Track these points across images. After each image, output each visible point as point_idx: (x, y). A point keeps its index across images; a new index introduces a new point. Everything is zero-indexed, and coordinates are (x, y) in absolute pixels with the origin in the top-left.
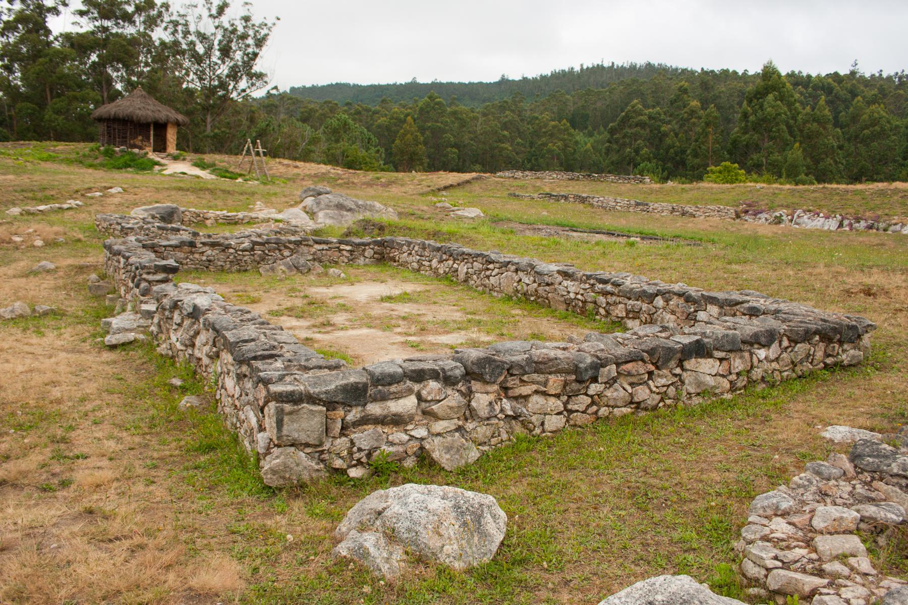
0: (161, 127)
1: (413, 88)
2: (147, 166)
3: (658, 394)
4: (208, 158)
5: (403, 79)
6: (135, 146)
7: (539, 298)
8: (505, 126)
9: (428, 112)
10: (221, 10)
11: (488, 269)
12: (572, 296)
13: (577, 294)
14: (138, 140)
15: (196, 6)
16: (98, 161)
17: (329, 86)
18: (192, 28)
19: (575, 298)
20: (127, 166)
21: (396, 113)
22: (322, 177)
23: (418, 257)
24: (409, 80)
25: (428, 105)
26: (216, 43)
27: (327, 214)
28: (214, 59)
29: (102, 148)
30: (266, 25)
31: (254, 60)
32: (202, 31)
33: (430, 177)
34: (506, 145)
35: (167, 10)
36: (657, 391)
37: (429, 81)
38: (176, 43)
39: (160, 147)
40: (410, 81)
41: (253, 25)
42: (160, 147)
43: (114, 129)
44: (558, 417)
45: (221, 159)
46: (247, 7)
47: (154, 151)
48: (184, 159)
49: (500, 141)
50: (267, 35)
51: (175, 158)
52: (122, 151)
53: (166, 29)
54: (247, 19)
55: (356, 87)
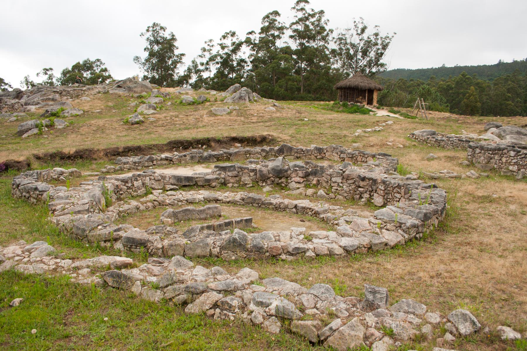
0: (371, 91)
1: (443, 71)
2: (365, 112)
5: (436, 64)
6: (358, 102)
8: (509, 91)
9: (461, 84)
10: (363, 30)
14: (360, 99)
16: (340, 110)
17: (393, 70)
18: (348, 41)
20: (355, 112)
21: (442, 84)
22: (448, 119)
24: (440, 66)
26: (360, 48)
27: (512, 137)
30: (388, 37)
31: (381, 56)
32: (353, 42)
33: (513, 119)
34: (510, 102)
35: (332, 33)
37: (453, 66)
39: (370, 102)
41: (381, 38)
42: (370, 102)
43: (348, 93)
45: (404, 110)
46: (377, 28)
48: (383, 109)
49: (506, 100)
50: (389, 43)
52: (351, 104)
53: (335, 42)
54: (376, 35)
55: (409, 70)
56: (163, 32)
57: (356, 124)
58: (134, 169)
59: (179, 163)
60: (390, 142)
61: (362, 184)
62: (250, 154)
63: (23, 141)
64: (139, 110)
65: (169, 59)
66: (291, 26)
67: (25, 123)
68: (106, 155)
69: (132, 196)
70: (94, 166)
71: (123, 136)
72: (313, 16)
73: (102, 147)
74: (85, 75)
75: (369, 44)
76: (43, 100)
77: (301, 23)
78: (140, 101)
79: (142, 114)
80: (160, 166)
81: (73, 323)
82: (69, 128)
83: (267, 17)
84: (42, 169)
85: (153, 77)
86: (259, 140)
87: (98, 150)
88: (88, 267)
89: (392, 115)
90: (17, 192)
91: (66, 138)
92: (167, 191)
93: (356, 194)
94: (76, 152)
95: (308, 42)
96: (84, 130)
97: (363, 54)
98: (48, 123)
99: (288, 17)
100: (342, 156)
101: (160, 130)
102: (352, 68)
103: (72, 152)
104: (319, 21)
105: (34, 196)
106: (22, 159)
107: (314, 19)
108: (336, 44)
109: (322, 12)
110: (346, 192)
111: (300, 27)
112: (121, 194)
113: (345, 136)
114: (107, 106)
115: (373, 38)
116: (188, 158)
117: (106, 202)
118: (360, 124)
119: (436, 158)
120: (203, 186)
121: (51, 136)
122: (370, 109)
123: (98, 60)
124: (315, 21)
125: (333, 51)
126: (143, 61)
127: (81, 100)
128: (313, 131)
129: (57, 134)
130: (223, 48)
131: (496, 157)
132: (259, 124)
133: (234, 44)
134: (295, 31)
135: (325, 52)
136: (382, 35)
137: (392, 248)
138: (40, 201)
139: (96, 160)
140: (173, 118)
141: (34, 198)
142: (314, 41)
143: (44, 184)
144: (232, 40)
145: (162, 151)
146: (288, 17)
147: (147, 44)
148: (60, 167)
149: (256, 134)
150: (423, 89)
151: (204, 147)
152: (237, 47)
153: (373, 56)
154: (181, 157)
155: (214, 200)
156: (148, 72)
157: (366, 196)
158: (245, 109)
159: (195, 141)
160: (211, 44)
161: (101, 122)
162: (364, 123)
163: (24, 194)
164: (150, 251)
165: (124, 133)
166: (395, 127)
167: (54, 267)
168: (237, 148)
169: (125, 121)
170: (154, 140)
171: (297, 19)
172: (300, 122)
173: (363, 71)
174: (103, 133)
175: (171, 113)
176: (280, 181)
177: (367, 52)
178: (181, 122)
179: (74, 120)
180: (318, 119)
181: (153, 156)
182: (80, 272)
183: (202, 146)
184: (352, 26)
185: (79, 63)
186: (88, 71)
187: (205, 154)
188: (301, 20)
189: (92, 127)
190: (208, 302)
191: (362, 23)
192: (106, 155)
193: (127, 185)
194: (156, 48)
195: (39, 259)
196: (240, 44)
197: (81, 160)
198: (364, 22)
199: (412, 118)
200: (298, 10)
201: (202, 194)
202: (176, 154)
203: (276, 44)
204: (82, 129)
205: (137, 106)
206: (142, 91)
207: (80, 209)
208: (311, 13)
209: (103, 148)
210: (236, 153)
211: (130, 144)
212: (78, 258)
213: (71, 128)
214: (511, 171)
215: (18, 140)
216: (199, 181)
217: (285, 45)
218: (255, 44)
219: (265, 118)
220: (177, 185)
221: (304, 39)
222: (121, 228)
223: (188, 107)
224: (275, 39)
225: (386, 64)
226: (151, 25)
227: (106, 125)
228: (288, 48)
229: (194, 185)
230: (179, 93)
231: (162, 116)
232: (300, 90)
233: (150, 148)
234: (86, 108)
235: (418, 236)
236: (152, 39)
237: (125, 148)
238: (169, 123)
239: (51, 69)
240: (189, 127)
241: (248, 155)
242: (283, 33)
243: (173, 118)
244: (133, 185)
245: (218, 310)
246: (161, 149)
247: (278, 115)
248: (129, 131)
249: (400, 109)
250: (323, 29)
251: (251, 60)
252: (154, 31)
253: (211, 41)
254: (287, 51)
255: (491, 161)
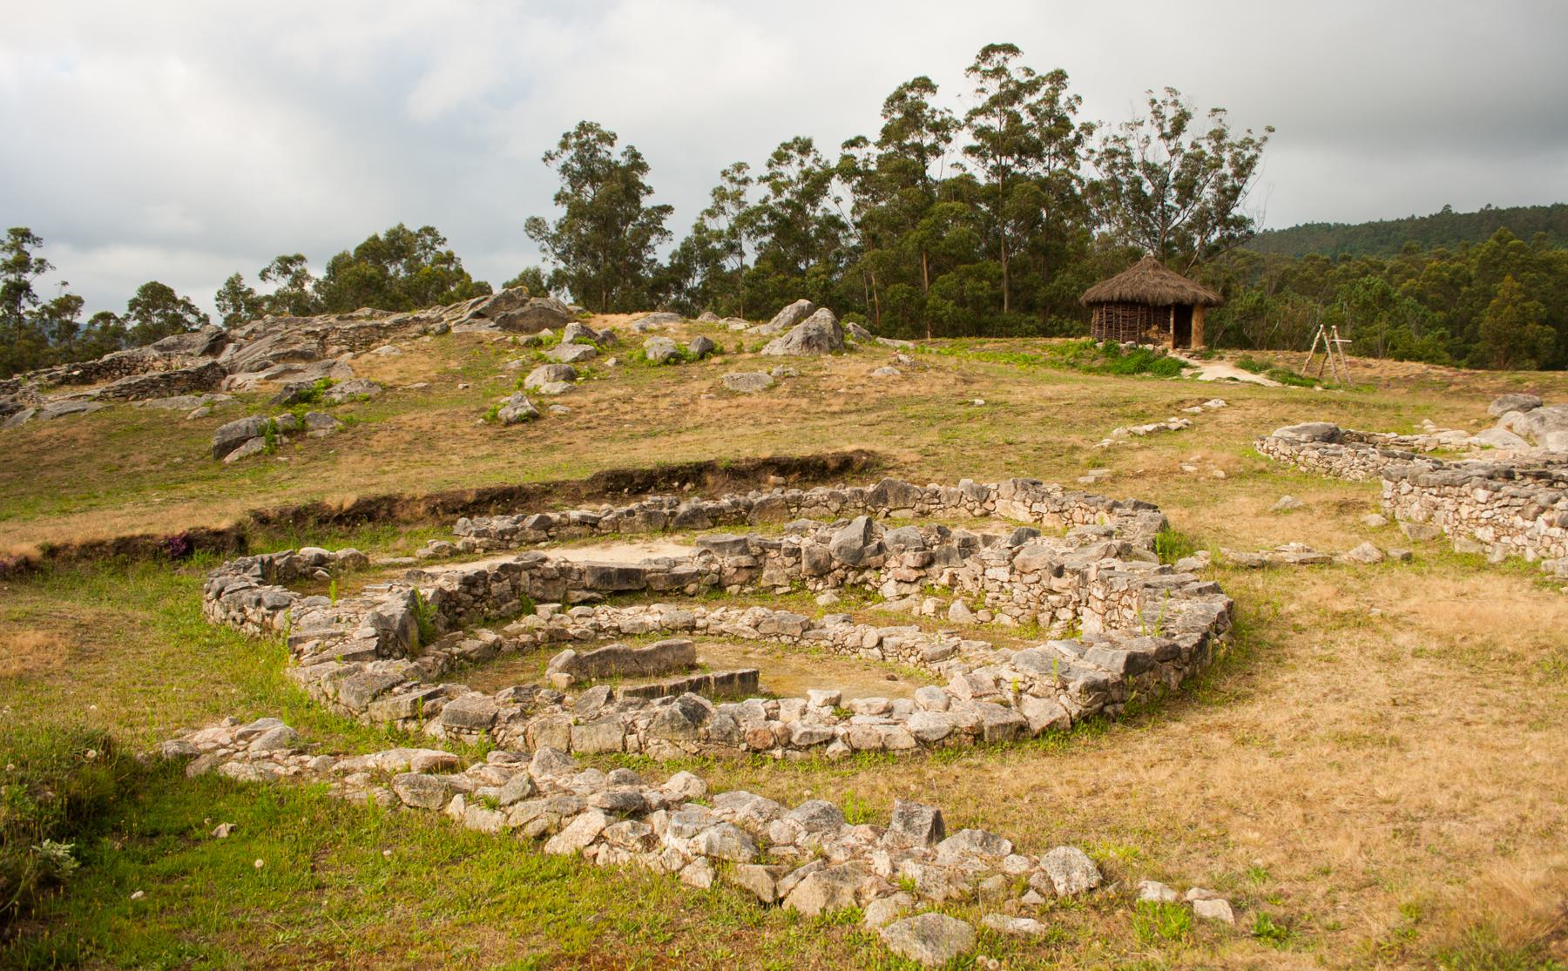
4: (1257, 356)
6: (1148, 340)
10: (1178, 127)
15: (1141, 124)
16: (1097, 364)
17: (1292, 230)
18: (1137, 158)
20: (1141, 368)
22: (1420, 383)
25: (1495, 252)
26: (1172, 176)
28: (1170, 202)
29: (1100, 345)
30: (1251, 142)
31: (1234, 198)
32: (1151, 161)
37: (1475, 208)
38: (1114, 181)
39: (1182, 340)
40: (1439, 211)
43: (1117, 316)
45: (1280, 358)
46: (1219, 115)
47: (1175, 347)
48: (1221, 358)
51: (1205, 357)
52: (1131, 348)
53: (1097, 163)
54: (1218, 135)
56: (608, 148)
57: (1116, 410)
58: (500, 548)
59: (615, 530)
60: (1191, 464)
61: (1056, 583)
62: (799, 507)
63: (226, 472)
64: (529, 381)
65: (625, 223)
66: (969, 120)
67: (230, 425)
68: (433, 511)
69: (487, 619)
70: (401, 543)
71: (482, 458)
72: (1032, 87)
73: (421, 492)
74: (392, 271)
75: (1196, 164)
76: (277, 358)
77: (996, 109)
78: (533, 353)
79: (534, 393)
80: (565, 540)
81: (331, 867)
82: (343, 436)
83: (900, 96)
84: (274, 550)
85: (582, 274)
86: (833, 464)
87: (413, 499)
88: (366, 770)
89: (1245, 376)
90: (217, 608)
91: (334, 463)
92: (573, 605)
93: (1042, 611)
94: (358, 505)
95: (1021, 163)
96: (381, 441)
97: (1180, 194)
98: (289, 424)
99: (957, 96)
100: (1036, 507)
101: (580, 438)
102: (1148, 234)
103: (347, 506)
104: (1052, 100)
105: (255, 618)
106: (224, 524)
107: (1039, 96)
108: (1101, 169)
109: (1059, 77)
110: (1018, 605)
111: (996, 123)
112: (460, 614)
113: (1074, 449)
114: (447, 371)
115: (1207, 148)
116: (639, 518)
117: (421, 633)
118: (1128, 410)
119: (1298, 509)
120: (665, 593)
121: (296, 458)
122: (1183, 358)
123: (429, 230)
124: (1040, 102)
125: (1095, 187)
126: (553, 230)
127: (378, 355)
128: (989, 435)
129: (313, 453)
130: (777, 189)
131: (1448, 504)
132: (847, 418)
133: (806, 175)
134: (981, 133)
135: (1072, 191)
136: (1235, 136)
137: (1037, 737)
138: (270, 630)
139: (407, 523)
140: (617, 405)
141: (254, 623)
142: (1040, 158)
143: (278, 589)
144: (802, 163)
145: (576, 497)
146: (957, 96)
147: (561, 183)
148: (317, 544)
149: (825, 451)
150: (1367, 288)
151: (688, 486)
152: (816, 185)
153: (1209, 197)
154: (621, 515)
155: (686, 628)
156: (567, 261)
157: (1066, 614)
158: (816, 374)
159: (662, 473)
160: (740, 177)
161: (426, 419)
162: (1140, 408)
163: (233, 613)
164: (499, 739)
165: (485, 449)
166: (1230, 417)
167: (296, 769)
168: (773, 490)
169: (489, 414)
170: (559, 469)
171: (985, 98)
172: (961, 410)
173: (1185, 241)
174: (431, 448)
175: (615, 392)
176: (860, 579)
177: (1192, 188)
178: (639, 416)
179: (357, 411)
180: (1012, 399)
181: (549, 514)
182: (347, 779)
183: (683, 484)
184: (1146, 113)
185: (376, 238)
186: (399, 259)
187: (683, 508)
188: (995, 101)
189: (401, 434)
190: (586, 831)
191: (1175, 103)
192: (433, 511)
193: (475, 591)
194: (589, 193)
195: (265, 753)
196: (828, 175)
197: (370, 525)
198: (1181, 100)
199: (1307, 383)
200: (985, 74)
201: (655, 614)
202: (604, 510)
203: (928, 173)
204: (376, 437)
205: (525, 370)
206: (540, 328)
207: (357, 649)
208: (1024, 80)
209: (425, 492)
210: (761, 504)
211: (494, 481)
212: (346, 754)
213: (349, 435)
214: (1480, 542)
215: (213, 471)
216: (655, 579)
217: (956, 173)
218: (870, 173)
219: (866, 399)
220: (599, 591)
221: (1010, 154)
222: (441, 691)
223: (662, 371)
224: (924, 160)
225: (1251, 221)
226: (573, 130)
227: (439, 427)
228: (967, 180)
229: (643, 590)
230: (643, 329)
231: (587, 399)
232: (1002, 302)
233: (547, 491)
234: (387, 379)
235: (1109, 709)
236: (577, 166)
237: (480, 494)
238: (605, 418)
239: (300, 259)
240: (658, 429)
241: (794, 510)
242: (948, 140)
243: (617, 405)
244: (489, 592)
245: (604, 847)
246: (575, 494)
247: (905, 388)
248: (499, 442)
249: (1269, 355)
250: (1064, 124)
251: (858, 219)
252: (582, 145)
253: (740, 167)
254: (961, 188)
255: (1437, 513)
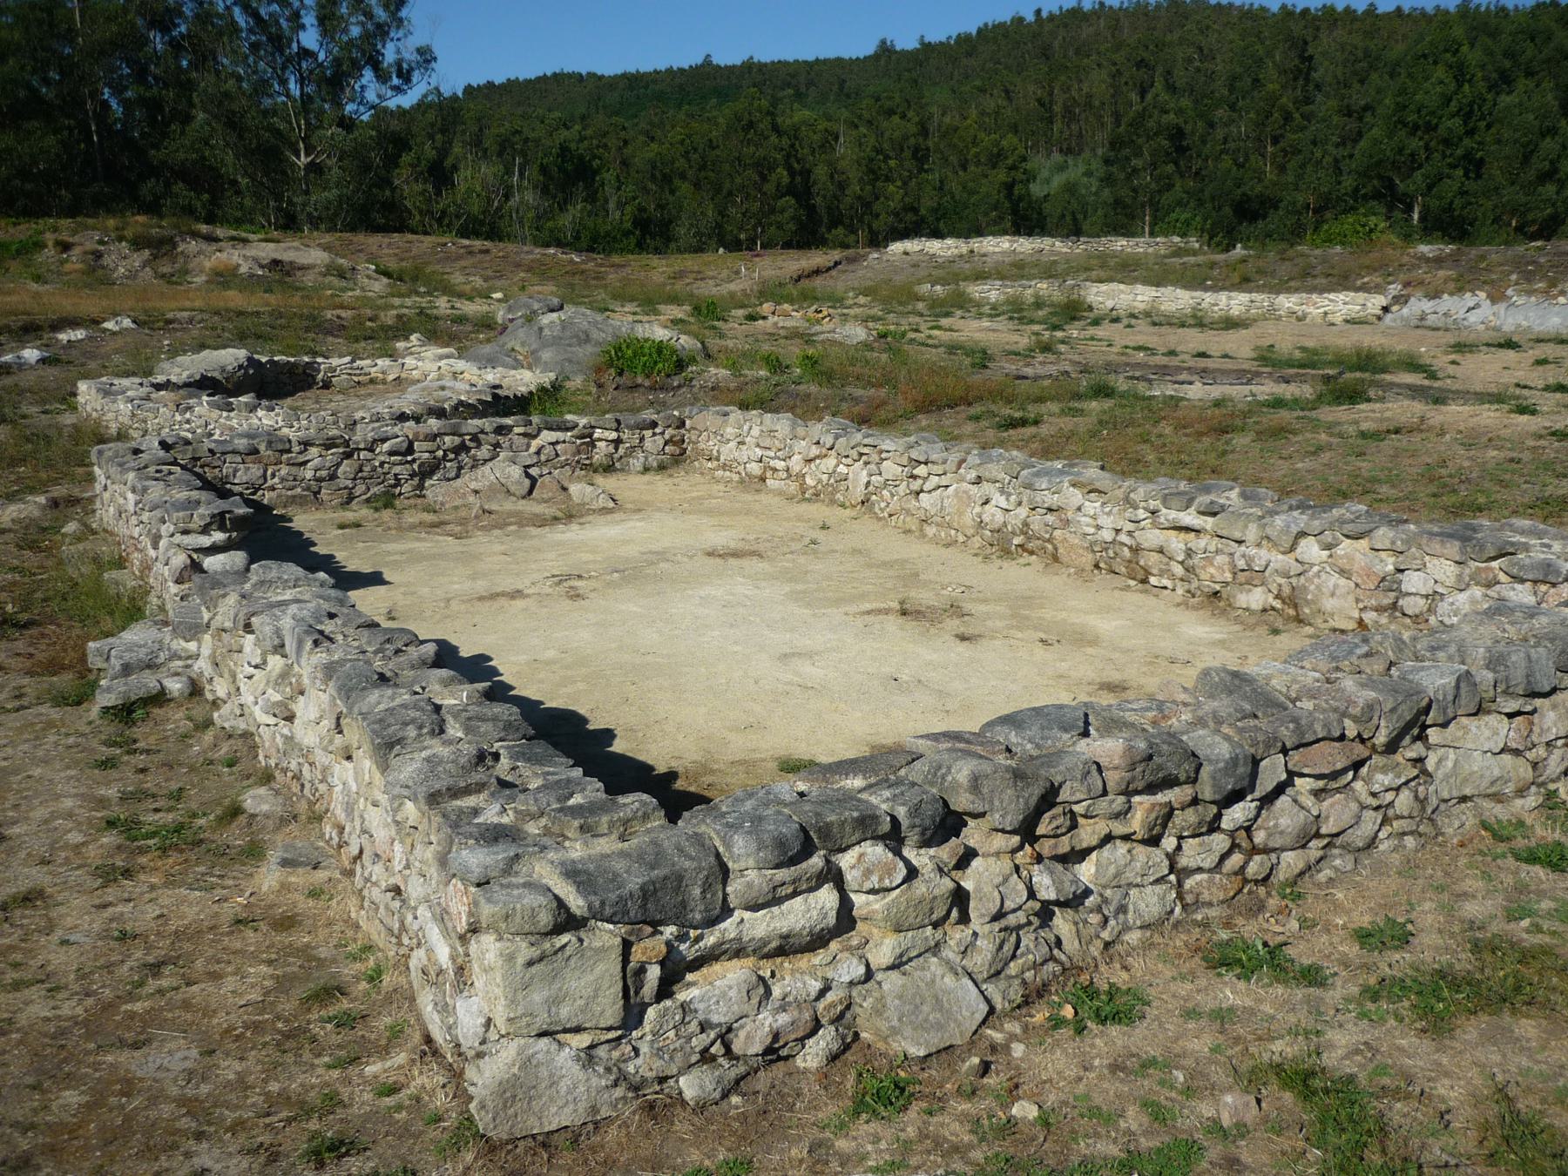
3: (1377, 808)
7: (1029, 539)
11: (914, 477)
12: (1107, 535)
13: (1118, 531)
17: (539, 79)
19: (1114, 542)
23: (759, 452)
24: (699, 60)
36: (1375, 803)
44: (1159, 889)
